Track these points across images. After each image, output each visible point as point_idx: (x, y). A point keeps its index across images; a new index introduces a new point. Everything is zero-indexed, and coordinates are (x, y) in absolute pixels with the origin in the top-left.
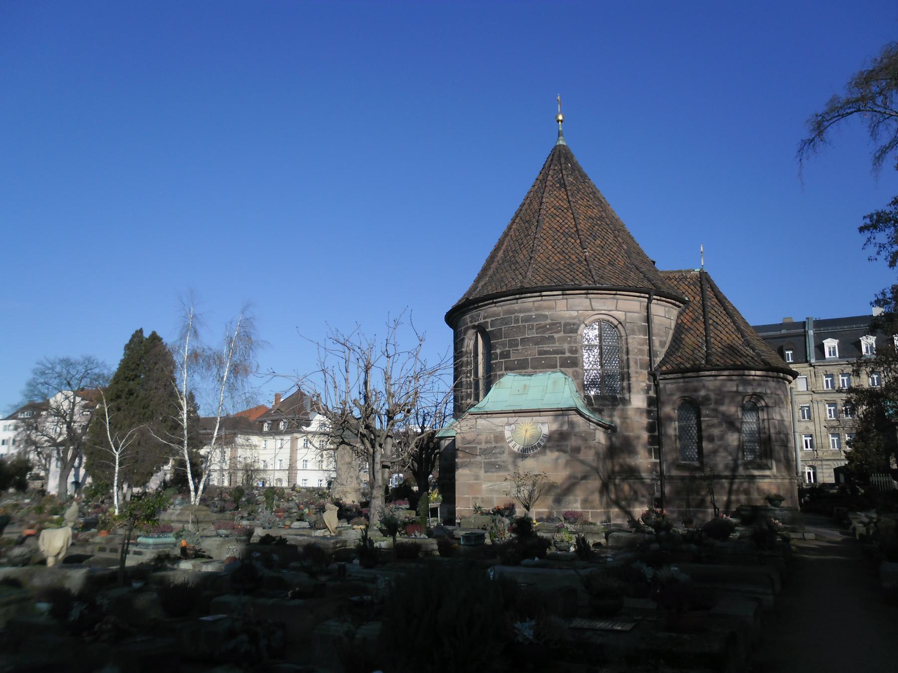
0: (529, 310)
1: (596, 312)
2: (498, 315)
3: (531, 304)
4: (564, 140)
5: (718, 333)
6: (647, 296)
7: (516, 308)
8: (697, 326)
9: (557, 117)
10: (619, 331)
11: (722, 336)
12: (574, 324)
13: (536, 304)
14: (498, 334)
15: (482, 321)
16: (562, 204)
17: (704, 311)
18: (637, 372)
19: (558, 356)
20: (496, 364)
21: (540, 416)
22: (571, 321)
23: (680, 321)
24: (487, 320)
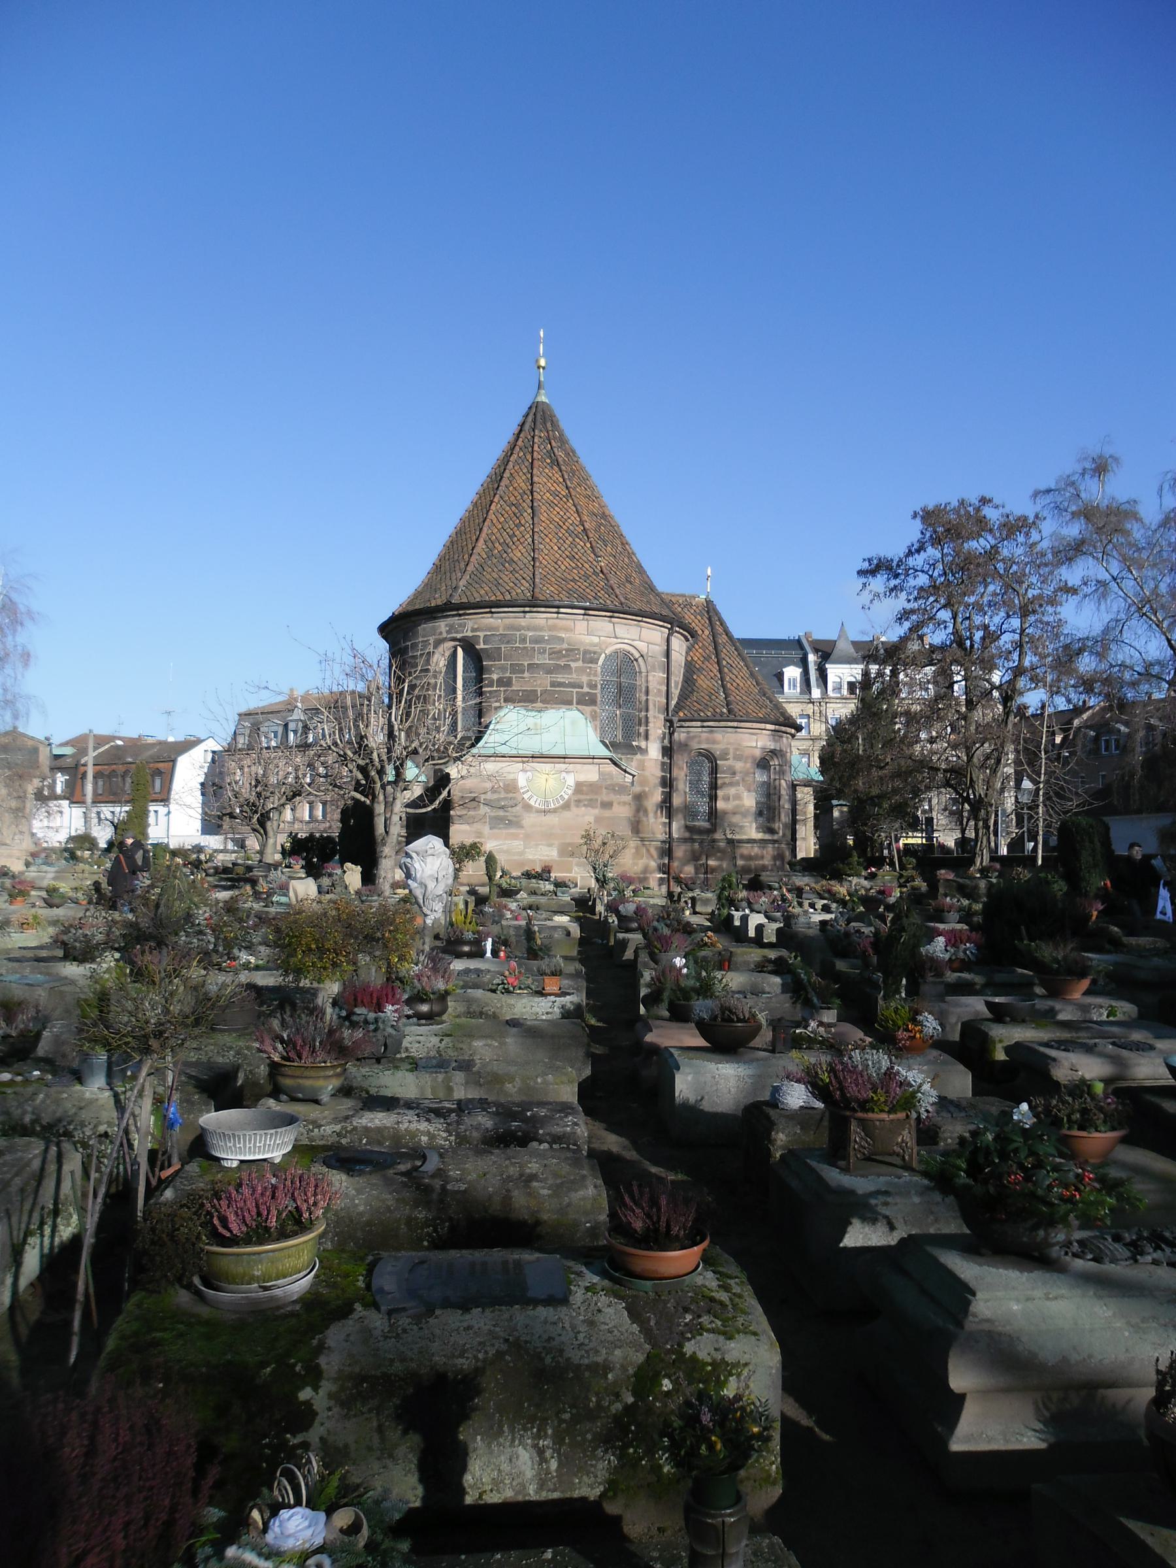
0: (541, 629)
1: (619, 640)
2: (497, 629)
3: (543, 622)
4: (547, 395)
5: (734, 677)
6: (669, 626)
7: (523, 624)
8: (710, 666)
9: (537, 361)
10: (639, 665)
11: (737, 681)
12: (595, 653)
13: (550, 622)
14: (495, 654)
15: (470, 634)
16: (558, 489)
17: (716, 648)
18: (655, 717)
19: (575, 690)
20: (490, 692)
21: (564, 763)
22: (592, 649)
23: (689, 659)
24: (478, 634)
